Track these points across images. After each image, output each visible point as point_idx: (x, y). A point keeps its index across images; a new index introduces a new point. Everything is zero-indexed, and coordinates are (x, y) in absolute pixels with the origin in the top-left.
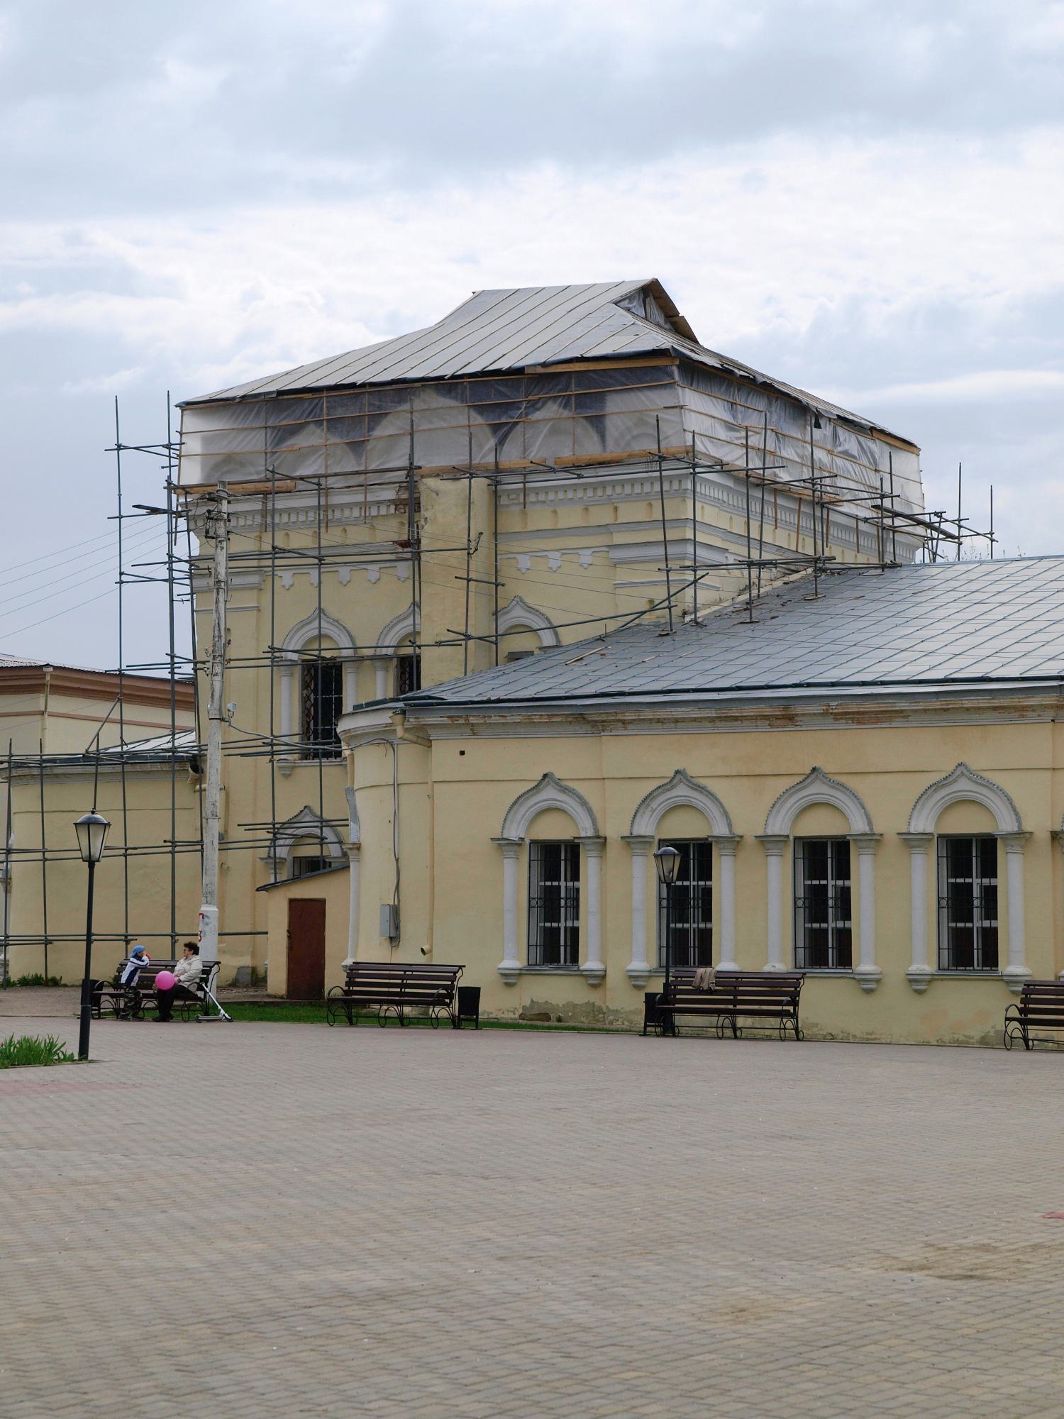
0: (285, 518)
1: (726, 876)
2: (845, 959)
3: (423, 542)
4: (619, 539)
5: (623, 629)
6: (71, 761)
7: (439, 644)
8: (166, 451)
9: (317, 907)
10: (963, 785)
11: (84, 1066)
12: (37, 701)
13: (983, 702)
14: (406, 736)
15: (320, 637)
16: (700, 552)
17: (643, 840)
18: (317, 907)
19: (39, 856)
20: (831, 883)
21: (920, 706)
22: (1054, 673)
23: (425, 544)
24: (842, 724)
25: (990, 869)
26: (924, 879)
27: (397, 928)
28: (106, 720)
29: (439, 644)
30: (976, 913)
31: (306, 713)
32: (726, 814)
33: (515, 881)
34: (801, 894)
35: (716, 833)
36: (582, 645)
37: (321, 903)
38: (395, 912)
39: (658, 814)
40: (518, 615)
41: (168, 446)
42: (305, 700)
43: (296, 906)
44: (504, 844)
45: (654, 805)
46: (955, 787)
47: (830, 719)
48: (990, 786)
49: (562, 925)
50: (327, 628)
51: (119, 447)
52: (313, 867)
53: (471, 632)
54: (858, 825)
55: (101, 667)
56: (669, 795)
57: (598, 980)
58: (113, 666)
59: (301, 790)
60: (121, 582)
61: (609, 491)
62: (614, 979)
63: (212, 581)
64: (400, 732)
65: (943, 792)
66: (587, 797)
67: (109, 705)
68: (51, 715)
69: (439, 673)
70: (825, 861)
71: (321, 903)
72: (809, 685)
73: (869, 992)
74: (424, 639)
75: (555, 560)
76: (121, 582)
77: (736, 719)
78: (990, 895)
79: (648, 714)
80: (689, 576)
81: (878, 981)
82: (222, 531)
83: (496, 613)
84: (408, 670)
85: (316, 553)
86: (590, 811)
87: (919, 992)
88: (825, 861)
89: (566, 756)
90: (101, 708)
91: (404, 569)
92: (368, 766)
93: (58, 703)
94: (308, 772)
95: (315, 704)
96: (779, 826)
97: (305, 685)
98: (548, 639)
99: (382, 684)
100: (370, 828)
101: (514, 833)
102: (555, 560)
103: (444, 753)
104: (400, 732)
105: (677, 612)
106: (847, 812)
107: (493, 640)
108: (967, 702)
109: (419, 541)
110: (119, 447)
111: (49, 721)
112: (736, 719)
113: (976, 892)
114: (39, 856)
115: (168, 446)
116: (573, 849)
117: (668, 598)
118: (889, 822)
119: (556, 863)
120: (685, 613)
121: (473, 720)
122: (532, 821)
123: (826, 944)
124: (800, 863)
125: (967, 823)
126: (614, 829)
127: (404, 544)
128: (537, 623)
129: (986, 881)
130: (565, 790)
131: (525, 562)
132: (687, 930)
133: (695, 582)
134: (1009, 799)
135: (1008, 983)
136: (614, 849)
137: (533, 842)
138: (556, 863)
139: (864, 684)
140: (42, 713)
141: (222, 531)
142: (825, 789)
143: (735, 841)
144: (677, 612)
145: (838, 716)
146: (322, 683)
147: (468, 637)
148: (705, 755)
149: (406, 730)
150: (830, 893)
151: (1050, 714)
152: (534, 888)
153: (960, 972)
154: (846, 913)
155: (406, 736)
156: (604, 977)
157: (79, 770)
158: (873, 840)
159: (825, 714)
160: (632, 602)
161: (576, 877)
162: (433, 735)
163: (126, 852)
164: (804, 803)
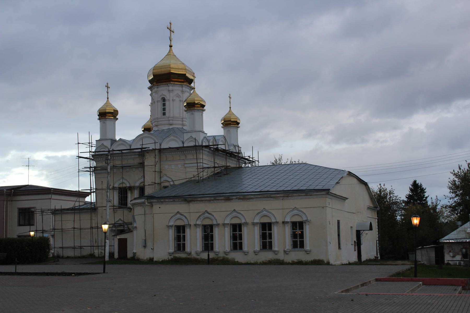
2: (241, 248)
4: (186, 162)
5: (187, 181)
6: (68, 209)
7: (149, 185)
9: (125, 240)
11: (104, 274)
13: (252, 197)
15: (123, 183)
16: (204, 165)
18: (125, 240)
20: (182, 234)
24: (240, 201)
28: (76, 201)
29: (149, 185)
30: (268, 238)
31: (119, 199)
32: (216, 219)
33: (172, 233)
36: (180, 184)
37: (126, 239)
38: (145, 240)
39: (201, 220)
40: (165, 178)
42: (119, 196)
44: (169, 227)
45: (201, 217)
46: (263, 213)
50: (124, 181)
52: (122, 232)
58: (77, 189)
59: (122, 216)
64: (147, 203)
65: (260, 214)
67: (76, 198)
69: (148, 191)
71: (126, 239)
72: (232, 193)
73: (308, 254)
74: (146, 184)
75: (173, 167)
80: (202, 170)
83: (161, 178)
84: (142, 189)
87: (256, 254)
89: (182, 207)
91: (140, 169)
92: (138, 211)
93: (54, 197)
95: (122, 197)
97: (119, 193)
98: (172, 183)
99: (136, 193)
100: (139, 223)
101: (171, 224)
102: (173, 167)
103: (156, 207)
104: (147, 203)
106: (302, 216)
108: (249, 197)
110: (78, 143)
113: (267, 234)
115: (89, 143)
116: (211, 227)
118: (249, 221)
119: (180, 230)
122: (175, 222)
124: (231, 229)
126: (192, 223)
127: (141, 163)
128: (170, 180)
130: (182, 215)
131: (166, 167)
134: (274, 215)
135: (274, 252)
136: (192, 227)
137: (175, 226)
138: (180, 230)
139: (243, 192)
142: (266, 213)
143: (218, 225)
145: (239, 199)
146: (123, 192)
147: (155, 183)
148: (211, 207)
151: (282, 198)
153: (235, 251)
157: (70, 212)
158: (246, 224)
159: (236, 198)
160: (190, 176)
161: (184, 240)
162: (154, 204)
163: (81, 229)
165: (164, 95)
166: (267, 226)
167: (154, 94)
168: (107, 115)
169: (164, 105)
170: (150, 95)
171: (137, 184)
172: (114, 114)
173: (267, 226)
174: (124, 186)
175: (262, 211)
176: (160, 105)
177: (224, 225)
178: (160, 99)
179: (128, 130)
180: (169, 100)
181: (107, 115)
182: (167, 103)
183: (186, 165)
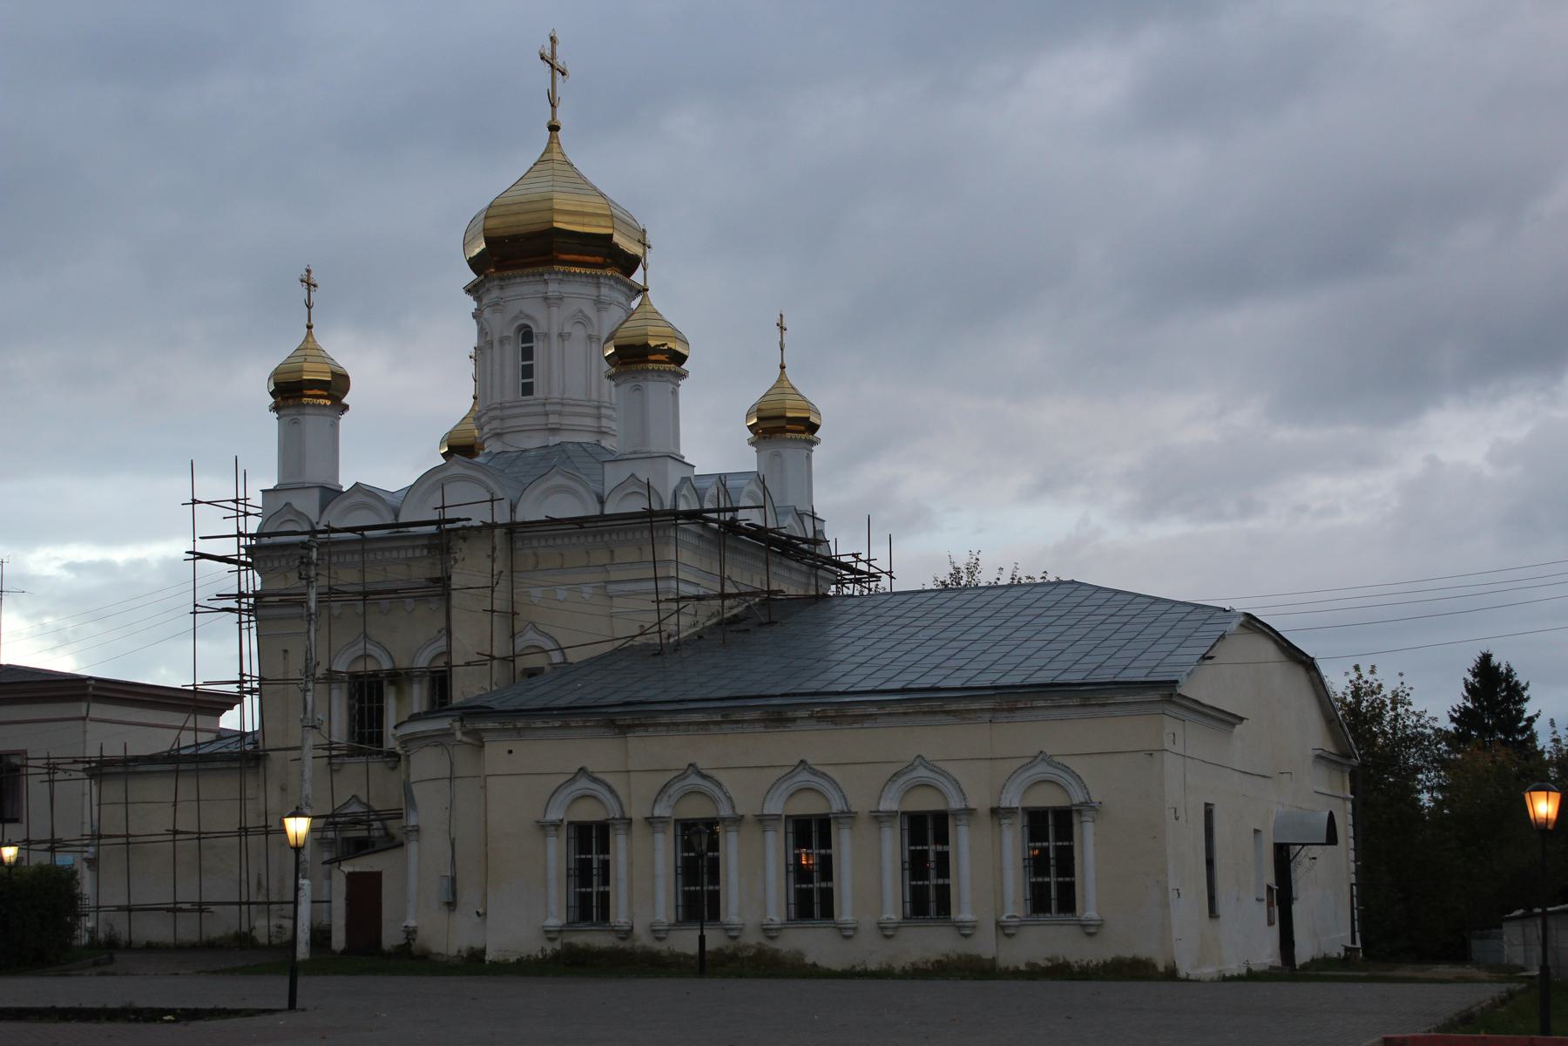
0: (372, 556)
1: (732, 850)
2: (828, 912)
3: (453, 579)
4: (614, 576)
6: (151, 759)
7: (468, 664)
8: (234, 506)
10: (922, 772)
12: (82, 708)
13: (873, 710)
14: (465, 739)
15: (366, 656)
17: (663, 820)
19: (123, 840)
21: (888, 710)
22: (987, 684)
23: (456, 581)
24: (823, 725)
25: (942, 838)
26: (663, 852)
27: (454, 894)
28: (182, 728)
29: (468, 664)
30: (932, 873)
33: (557, 853)
34: (907, 858)
35: (1076, 801)
37: (376, 878)
40: (528, 638)
41: (236, 501)
42: (351, 708)
43: (352, 878)
44: (544, 827)
45: (671, 791)
46: (914, 774)
47: (814, 722)
48: (943, 773)
49: (595, 889)
50: (372, 650)
51: (194, 502)
52: (361, 847)
53: (496, 654)
54: (837, 806)
55: (176, 683)
56: (574, 788)
57: (628, 933)
60: (195, 613)
61: (606, 538)
62: (638, 930)
63: (305, 612)
64: (459, 735)
66: (614, 786)
67: (183, 716)
68: (92, 720)
69: (465, 688)
70: (811, 832)
72: (794, 695)
73: (847, 937)
74: (457, 659)
75: (562, 594)
76: (195, 613)
77: (737, 722)
78: (943, 859)
79: (665, 719)
80: (674, 606)
81: (855, 929)
82: (313, 573)
83: (513, 636)
84: (440, 682)
85: (360, 589)
86: (617, 797)
88: (811, 832)
89: (597, 752)
90: (177, 718)
92: (425, 764)
93: (97, 710)
94: (355, 767)
96: (889, 804)
97: (351, 696)
98: (556, 657)
99: (418, 697)
100: (428, 812)
103: (495, 751)
104: (459, 735)
105: (664, 635)
107: (510, 660)
109: (449, 578)
110: (194, 502)
111: (90, 725)
112: (737, 722)
113: (932, 857)
114: (123, 840)
115: (236, 501)
116: (603, 829)
117: (659, 623)
118: (861, 804)
119: (590, 840)
120: (669, 636)
121: (519, 725)
123: (812, 898)
124: (790, 836)
125: (925, 803)
126: (637, 812)
128: (549, 645)
129: (939, 848)
132: (811, 890)
133: (678, 611)
135: (959, 928)
136: (637, 829)
138: (590, 840)
140: (84, 719)
141: (313, 573)
144: (664, 635)
146: (367, 694)
147: (492, 658)
149: (464, 734)
150: (595, 865)
151: (988, 716)
152: (907, 854)
154: (605, 881)
155: (465, 739)
156: (631, 930)
158: (849, 816)
159: (811, 717)
162: (486, 737)
163: (200, 836)
164: (575, 795)
165: (529, 317)
166: (930, 825)
167: (487, 313)
168: (307, 394)
169: (528, 354)
170: (474, 316)
171: (422, 661)
172: (335, 388)
173: (930, 825)
174: (371, 666)
175: (911, 767)
176: (510, 357)
177: (762, 820)
178: (510, 332)
179: (392, 443)
180: (546, 336)
181: (307, 394)
182: (538, 347)
183: (611, 587)
